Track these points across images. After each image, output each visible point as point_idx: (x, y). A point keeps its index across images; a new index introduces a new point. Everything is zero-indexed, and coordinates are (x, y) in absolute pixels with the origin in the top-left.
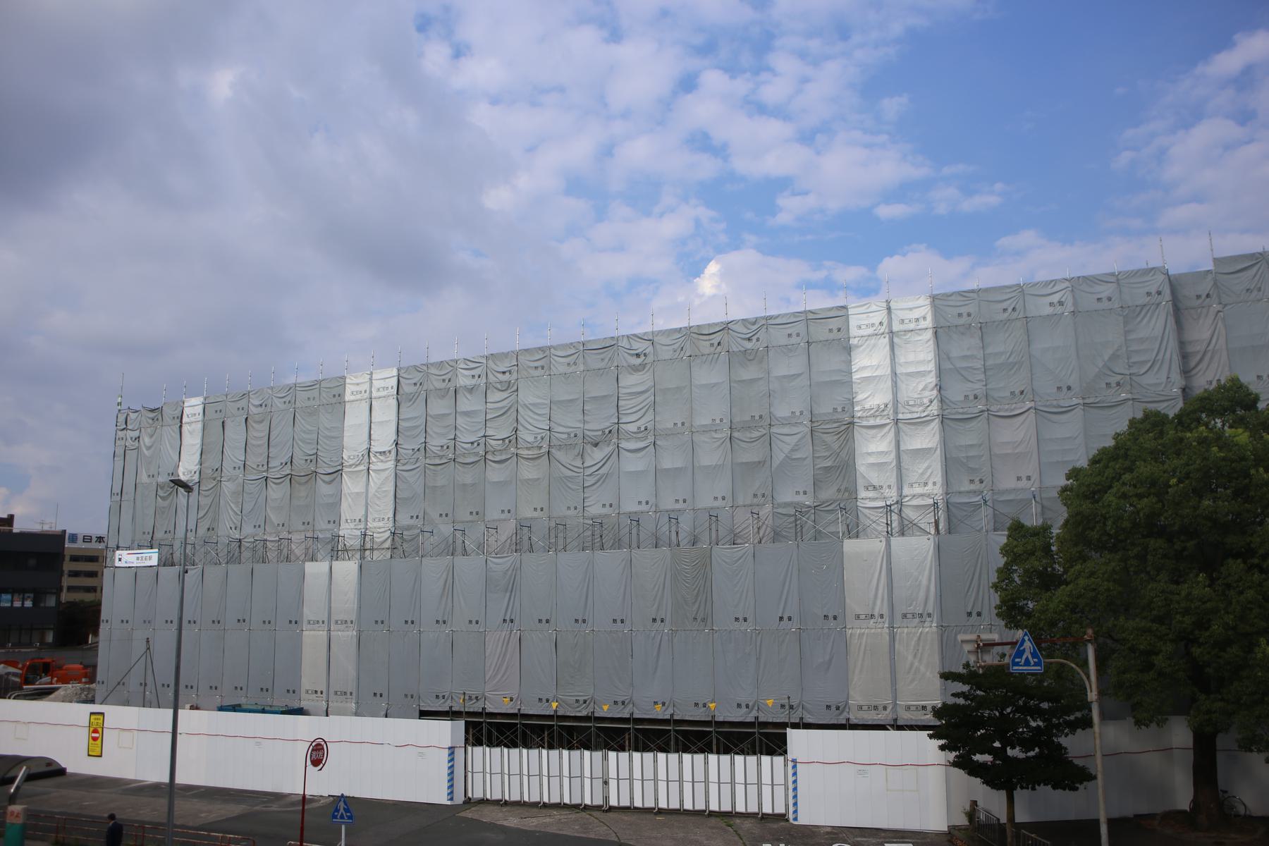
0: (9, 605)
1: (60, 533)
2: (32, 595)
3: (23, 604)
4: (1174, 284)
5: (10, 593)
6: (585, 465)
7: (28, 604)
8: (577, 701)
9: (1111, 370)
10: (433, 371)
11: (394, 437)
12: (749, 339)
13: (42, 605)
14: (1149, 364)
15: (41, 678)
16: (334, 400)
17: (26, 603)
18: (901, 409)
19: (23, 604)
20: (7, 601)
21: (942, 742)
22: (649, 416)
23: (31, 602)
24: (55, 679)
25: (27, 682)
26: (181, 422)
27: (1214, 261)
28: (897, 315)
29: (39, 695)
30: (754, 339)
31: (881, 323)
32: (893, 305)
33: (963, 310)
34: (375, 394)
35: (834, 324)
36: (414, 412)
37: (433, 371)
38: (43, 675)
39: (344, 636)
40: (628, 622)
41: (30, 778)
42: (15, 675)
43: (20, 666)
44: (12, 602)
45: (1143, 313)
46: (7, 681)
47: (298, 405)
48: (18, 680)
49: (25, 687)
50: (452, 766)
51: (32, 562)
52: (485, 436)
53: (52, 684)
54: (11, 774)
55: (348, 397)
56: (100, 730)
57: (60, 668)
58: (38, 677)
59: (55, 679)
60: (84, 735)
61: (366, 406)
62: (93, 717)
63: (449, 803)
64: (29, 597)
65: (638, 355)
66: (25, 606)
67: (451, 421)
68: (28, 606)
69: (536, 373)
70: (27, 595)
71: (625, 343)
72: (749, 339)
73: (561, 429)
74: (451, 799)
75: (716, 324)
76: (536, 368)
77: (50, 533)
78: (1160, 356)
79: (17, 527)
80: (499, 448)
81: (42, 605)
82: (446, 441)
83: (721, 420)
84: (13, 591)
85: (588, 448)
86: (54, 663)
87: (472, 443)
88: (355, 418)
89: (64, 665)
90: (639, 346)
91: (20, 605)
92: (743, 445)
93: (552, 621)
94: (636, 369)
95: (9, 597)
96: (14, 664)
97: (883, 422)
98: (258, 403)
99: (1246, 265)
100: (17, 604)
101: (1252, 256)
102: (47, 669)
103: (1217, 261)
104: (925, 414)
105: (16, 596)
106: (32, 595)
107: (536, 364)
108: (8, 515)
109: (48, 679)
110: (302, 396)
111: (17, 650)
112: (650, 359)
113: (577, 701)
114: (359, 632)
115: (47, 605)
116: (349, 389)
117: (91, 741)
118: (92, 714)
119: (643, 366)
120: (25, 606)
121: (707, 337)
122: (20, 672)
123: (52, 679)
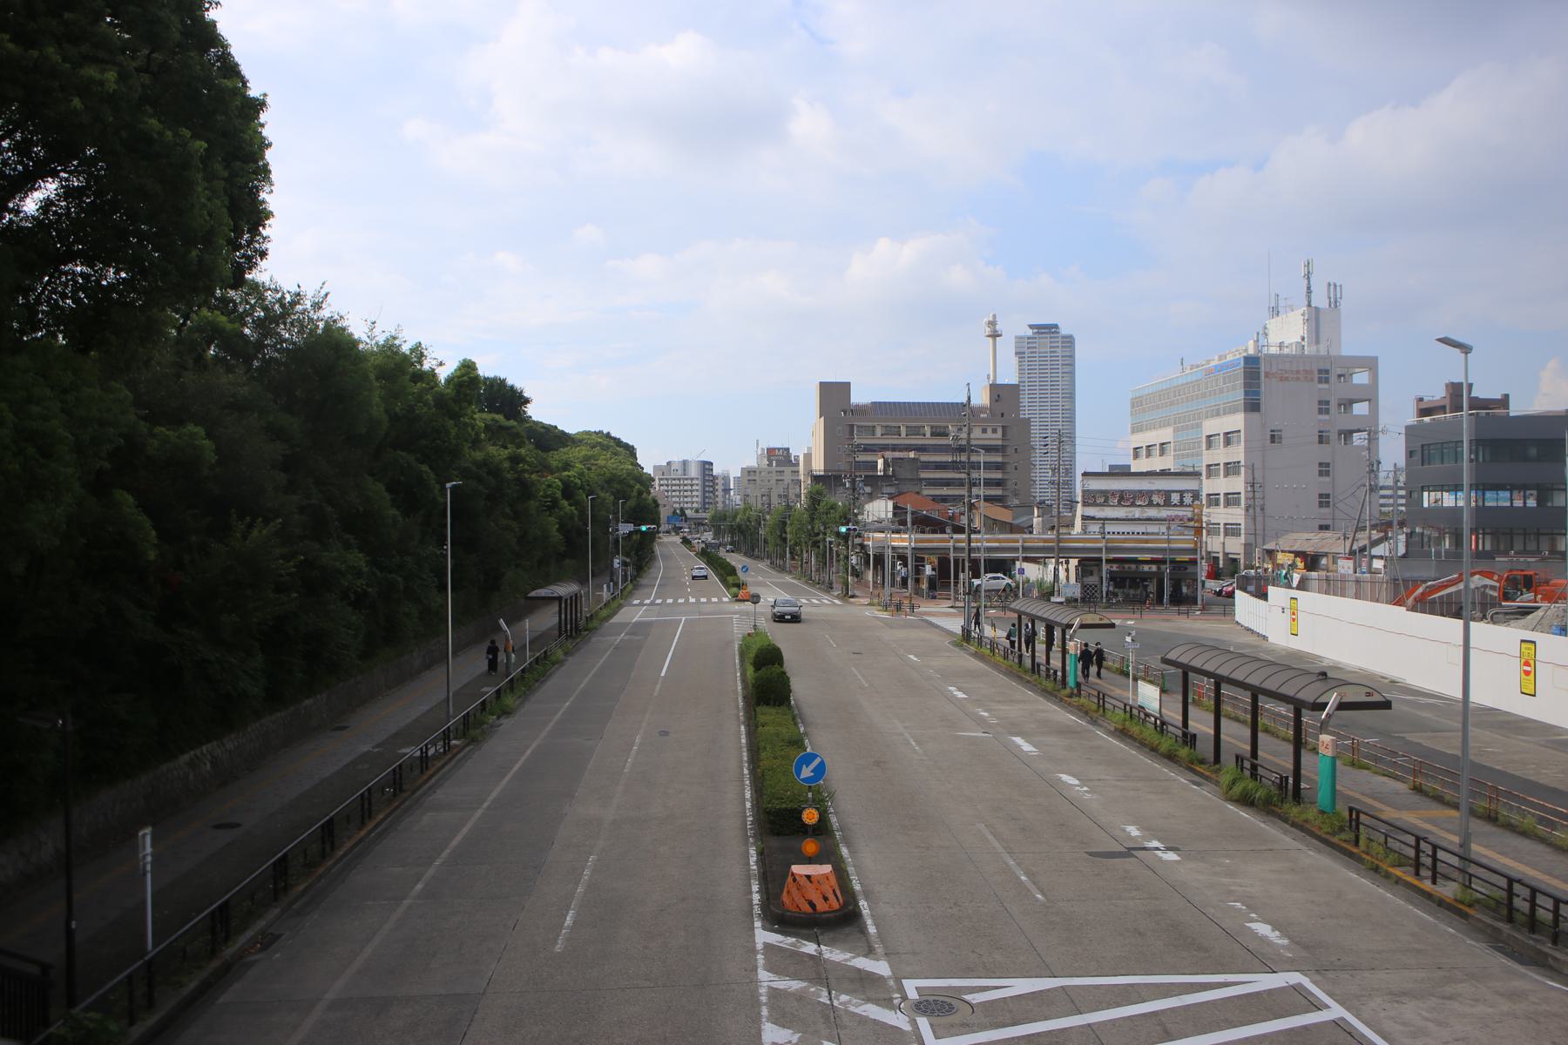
0: (1508, 504)
1: (1564, 414)
2: (1535, 492)
3: (1525, 503)
5: (1508, 490)
7: (1532, 503)
13: (1549, 504)
15: (1522, 594)
17: (1528, 502)
19: (1525, 503)
21: (261, 228)
23: (1535, 502)
24: (1540, 596)
25: (1506, 597)
29: (1522, 615)
38: (1524, 590)
41: (1342, 706)
42: (1493, 588)
43: (1496, 577)
44: (1512, 500)
46: (1484, 595)
48: (1496, 594)
49: (1503, 603)
51: (1533, 452)
53: (1536, 602)
56: (1532, 662)
57: (1547, 583)
58: (1519, 593)
59: (1540, 596)
60: (1516, 665)
62: (1524, 645)
64: (1532, 495)
66: (1515, 505)
68: (1531, 505)
70: (1528, 492)
77: (1551, 414)
79: (1515, 409)
81: (1549, 504)
84: (1512, 488)
86: (1537, 577)
89: (1551, 580)
91: (1521, 505)
95: (1507, 494)
96: (1489, 575)
100: (1518, 503)
102: (1528, 583)
105: (1515, 493)
106: (1535, 492)
108: (1502, 395)
109: (1531, 596)
111: (1522, 559)
115: (1556, 504)
117: (1523, 676)
118: (1522, 641)
120: (1528, 505)
122: (1498, 585)
123: (1536, 596)
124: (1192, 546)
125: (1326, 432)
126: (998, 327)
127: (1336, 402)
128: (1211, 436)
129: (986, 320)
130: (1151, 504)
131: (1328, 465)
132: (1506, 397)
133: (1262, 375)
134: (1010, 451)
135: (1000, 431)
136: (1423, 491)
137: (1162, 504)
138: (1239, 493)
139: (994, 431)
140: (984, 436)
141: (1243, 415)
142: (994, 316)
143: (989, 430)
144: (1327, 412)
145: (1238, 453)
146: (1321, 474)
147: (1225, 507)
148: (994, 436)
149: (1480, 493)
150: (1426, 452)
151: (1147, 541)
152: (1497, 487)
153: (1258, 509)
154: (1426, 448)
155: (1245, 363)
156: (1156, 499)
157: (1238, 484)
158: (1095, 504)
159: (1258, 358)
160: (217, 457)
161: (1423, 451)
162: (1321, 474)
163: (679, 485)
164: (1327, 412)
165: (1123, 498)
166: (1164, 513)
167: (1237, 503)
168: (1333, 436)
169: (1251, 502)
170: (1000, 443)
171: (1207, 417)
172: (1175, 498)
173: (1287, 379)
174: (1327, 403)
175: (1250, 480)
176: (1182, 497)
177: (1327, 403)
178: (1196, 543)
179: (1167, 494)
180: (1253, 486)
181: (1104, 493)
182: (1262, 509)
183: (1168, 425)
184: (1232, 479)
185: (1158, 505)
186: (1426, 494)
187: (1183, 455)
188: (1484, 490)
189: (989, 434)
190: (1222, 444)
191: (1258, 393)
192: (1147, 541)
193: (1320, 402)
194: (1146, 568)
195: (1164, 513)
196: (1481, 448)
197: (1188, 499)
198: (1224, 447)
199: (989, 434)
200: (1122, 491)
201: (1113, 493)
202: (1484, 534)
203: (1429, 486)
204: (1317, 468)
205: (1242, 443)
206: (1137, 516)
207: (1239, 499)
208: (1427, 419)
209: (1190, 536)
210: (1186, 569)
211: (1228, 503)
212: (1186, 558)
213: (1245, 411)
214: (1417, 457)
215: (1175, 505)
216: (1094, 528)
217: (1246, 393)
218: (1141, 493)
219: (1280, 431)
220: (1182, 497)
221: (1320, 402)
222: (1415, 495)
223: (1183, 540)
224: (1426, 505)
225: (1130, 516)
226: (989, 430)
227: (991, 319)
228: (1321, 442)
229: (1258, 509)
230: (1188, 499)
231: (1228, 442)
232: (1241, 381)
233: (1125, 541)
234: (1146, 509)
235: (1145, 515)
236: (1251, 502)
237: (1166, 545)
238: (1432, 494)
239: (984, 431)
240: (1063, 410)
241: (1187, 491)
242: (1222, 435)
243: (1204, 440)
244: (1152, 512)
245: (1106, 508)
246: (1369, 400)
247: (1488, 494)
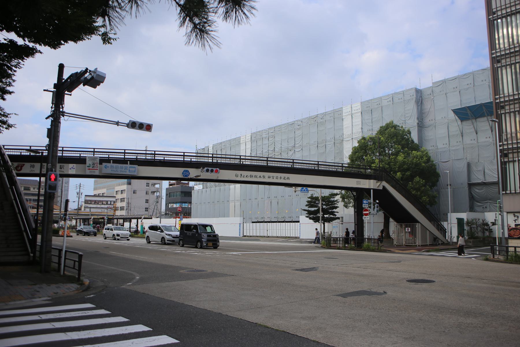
4: (418, 92)
6: (288, 156)
8: (282, 217)
9: (401, 120)
10: (258, 133)
11: (250, 152)
12: (322, 119)
14: (409, 117)
16: (238, 143)
18: (353, 135)
20: (187, 205)
22: (301, 142)
26: (208, 151)
27: (334, 112)
28: (353, 109)
30: (323, 118)
31: (350, 111)
32: (352, 106)
33: (368, 106)
34: (247, 141)
35: (339, 113)
36: (254, 144)
37: (258, 133)
39: (238, 204)
40: (292, 196)
45: (409, 102)
47: (270, 134)
50: (240, 228)
52: (268, 150)
54: (141, 217)
55: (241, 142)
61: (351, 116)
63: (239, 236)
65: (299, 125)
67: (261, 147)
69: (279, 132)
71: (296, 122)
72: (322, 119)
73: (284, 147)
74: (240, 236)
75: (314, 116)
76: (278, 131)
78: (412, 114)
80: (271, 153)
82: (260, 152)
83: (350, 134)
85: (289, 151)
87: (266, 152)
88: (347, 123)
90: (300, 123)
92: (320, 148)
93: (277, 197)
94: (299, 129)
97: (350, 139)
98: (223, 145)
99: (439, 84)
101: (442, 81)
103: (433, 83)
104: (358, 136)
107: (279, 130)
110: (232, 142)
112: (301, 126)
113: (282, 217)
114: (241, 203)
116: (241, 140)
119: (300, 128)
121: (313, 119)
124: (113, 214)
125: (148, 191)
127: (151, 184)
128: (117, 191)
130: (103, 204)
131: (148, 200)
136: (169, 204)
137: (106, 204)
138: (124, 207)
141: (126, 186)
144: (149, 186)
145: (124, 195)
146: (146, 202)
147: (120, 211)
149: (181, 204)
150: (170, 195)
152: (185, 203)
153: (129, 210)
154: (170, 193)
156: (104, 203)
157: (124, 204)
158: (88, 203)
161: (170, 194)
162: (146, 202)
164: (149, 186)
165: (96, 202)
166: (106, 206)
167: (123, 209)
168: (150, 192)
169: (127, 208)
171: (116, 186)
172: (109, 203)
174: (149, 184)
175: (127, 202)
176: (111, 202)
177: (149, 184)
178: (114, 213)
179: (107, 201)
180: (128, 203)
181: (91, 201)
182: (130, 210)
183: (105, 188)
184: (122, 203)
185: (105, 204)
186: (170, 204)
187: (112, 188)
188: (182, 203)
190: (120, 202)
192: (101, 213)
194: (101, 220)
195: (106, 206)
196: (182, 193)
197: (112, 203)
198: (120, 202)
200: (95, 200)
201: (93, 201)
202: (182, 213)
203: (170, 203)
204: (145, 201)
205: (126, 193)
206: (99, 207)
207: (124, 208)
208: (171, 187)
209: (112, 212)
210: (111, 221)
211: (121, 210)
212: (111, 217)
213: (127, 184)
214: (168, 196)
215: (109, 204)
216: (88, 210)
218: (100, 201)
219: (136, 190)
220: (111, 202)
222: (167, 205)
223: (111, 213)
224: (170, 207)
225: (97, 207)
228: (146, 194)
229: (129, 210)
230: (112, 203)
231: (122, 193)
233: (96, 212)
234: (102, 205)
235: (101, 207)
236: (127, 208)
237: (106, 214)
238: (171, 204)
240: (65, 187)
241: (112, 201)
242: (120, 191)
243: (115, 192)
244: (103, 206)
245: (91, 205)
246: (159, 184)
247: (183, 204)
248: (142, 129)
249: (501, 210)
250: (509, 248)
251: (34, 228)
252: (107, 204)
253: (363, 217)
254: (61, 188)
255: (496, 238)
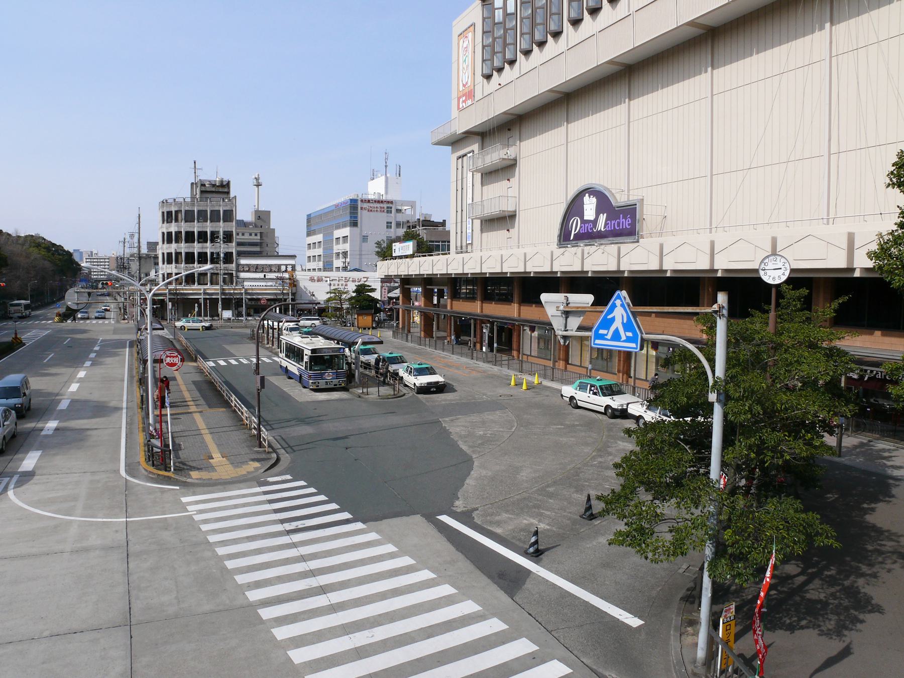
126: (260, 181)
129: (254, 177)
132: (444, 221)
133: (359, 208)
134: (264, 245)
135: (259, 235)
139: (256, 235)
140: (251, 237)
142: (258, 175)
143: (253, 235)
148: (256, 237)
151: (266, 289)
155: (351, 202)
156: (273, 269)
159: (357, 200)
160: (808, 291)
163: (98, 262)
170: (259, 241)
172: (283, 268)
173: (371, 211)
176: (286, 267)
177: (391, 223)
179: (279, 266)
189: (253, 237)
191: (356, 217)
192: (266, 289)
193: (387, 223)
199: (253, 237)
217: (351, 217)
221: (387, 223)
226: (253, 235)
227: (257, 177)
232: (348, 211)
239: (251, 235)
241: (289, 265)
248: (711, 628)
249: (622, 298)
250: (484, 73)
251: (721, 290)
252: (279, 271)
253: (618, 292)
254: (319, 251)
255: (697, 304)
